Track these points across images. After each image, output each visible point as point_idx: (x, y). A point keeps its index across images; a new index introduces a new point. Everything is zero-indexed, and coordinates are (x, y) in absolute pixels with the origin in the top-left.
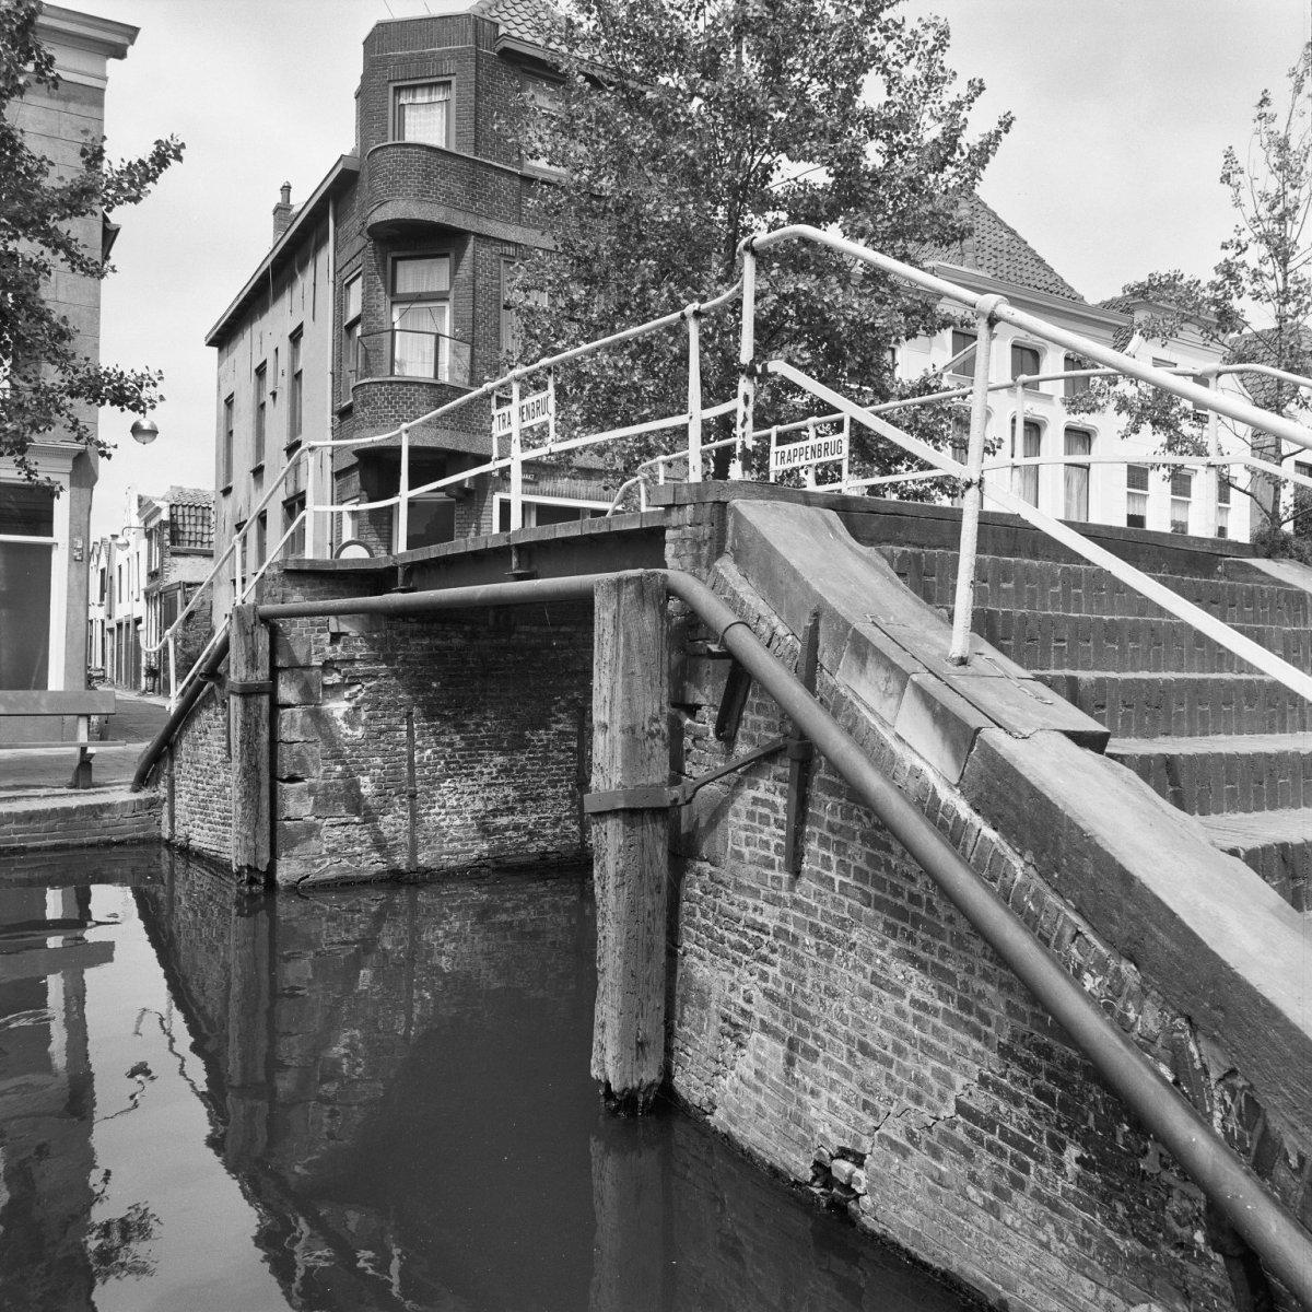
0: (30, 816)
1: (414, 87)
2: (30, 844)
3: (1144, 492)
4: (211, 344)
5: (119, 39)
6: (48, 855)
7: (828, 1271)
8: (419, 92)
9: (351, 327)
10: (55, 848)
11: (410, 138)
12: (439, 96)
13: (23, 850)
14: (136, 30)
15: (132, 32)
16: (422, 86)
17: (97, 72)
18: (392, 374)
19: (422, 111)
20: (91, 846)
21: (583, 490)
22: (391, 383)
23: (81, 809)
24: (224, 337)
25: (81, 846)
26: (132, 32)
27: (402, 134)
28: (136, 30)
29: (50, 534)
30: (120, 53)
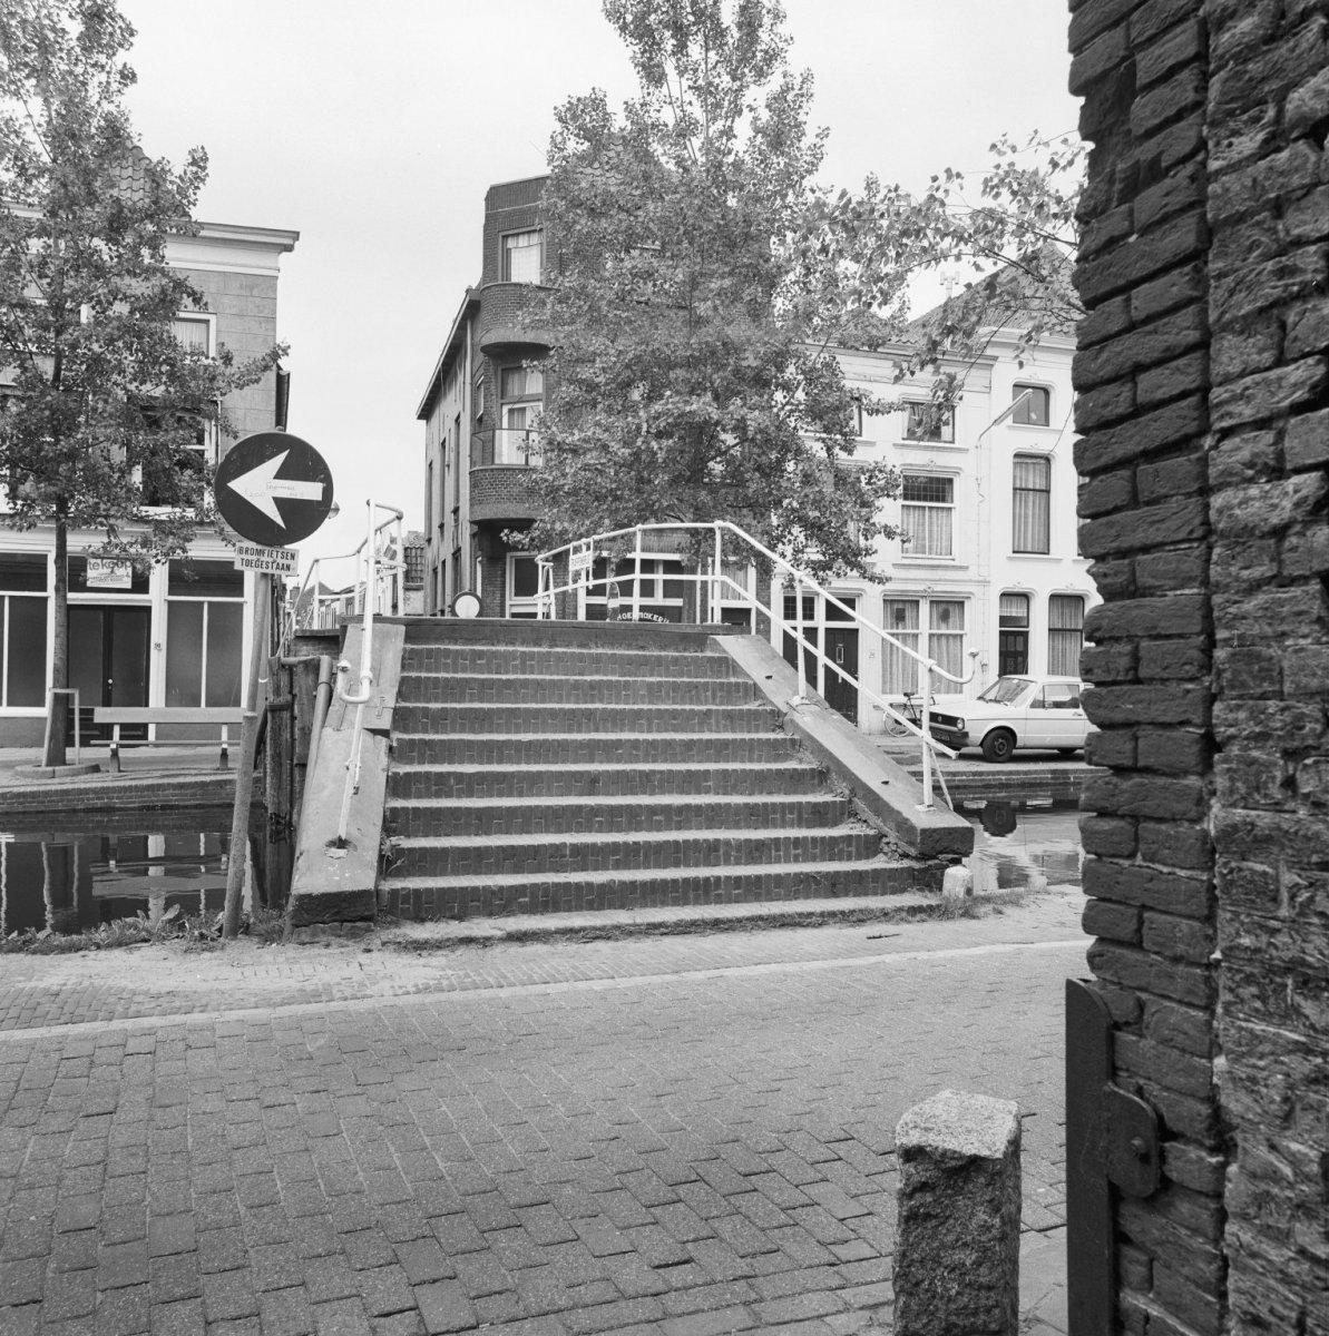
0: (181, 786)
1: (518, 235)
2: (181, 803)
3: (699, 586)
4: (420, 417)
5: (289, 241)
6: (194, 811)
7: (384, 944)
8: (521, 238)
9: (480, 420)
10: (196, 807)
11: (514, 279)
12: (535, 238)
13: (178, 807)
14: (298, 233)
15: (296, 235)
16: (523, 233)
17: (273, 265)
18: (493, 463)
19: (523, 252)
20: (218, 806)
21: (656, 545)
22: (492, 470)
23: (212, 783)
24: (426, 412)
25: (213, 806)
26: (296, 235)
27: (507, 275)
28: (298, 233)
29: (241, 595)
30: (289, 248)
